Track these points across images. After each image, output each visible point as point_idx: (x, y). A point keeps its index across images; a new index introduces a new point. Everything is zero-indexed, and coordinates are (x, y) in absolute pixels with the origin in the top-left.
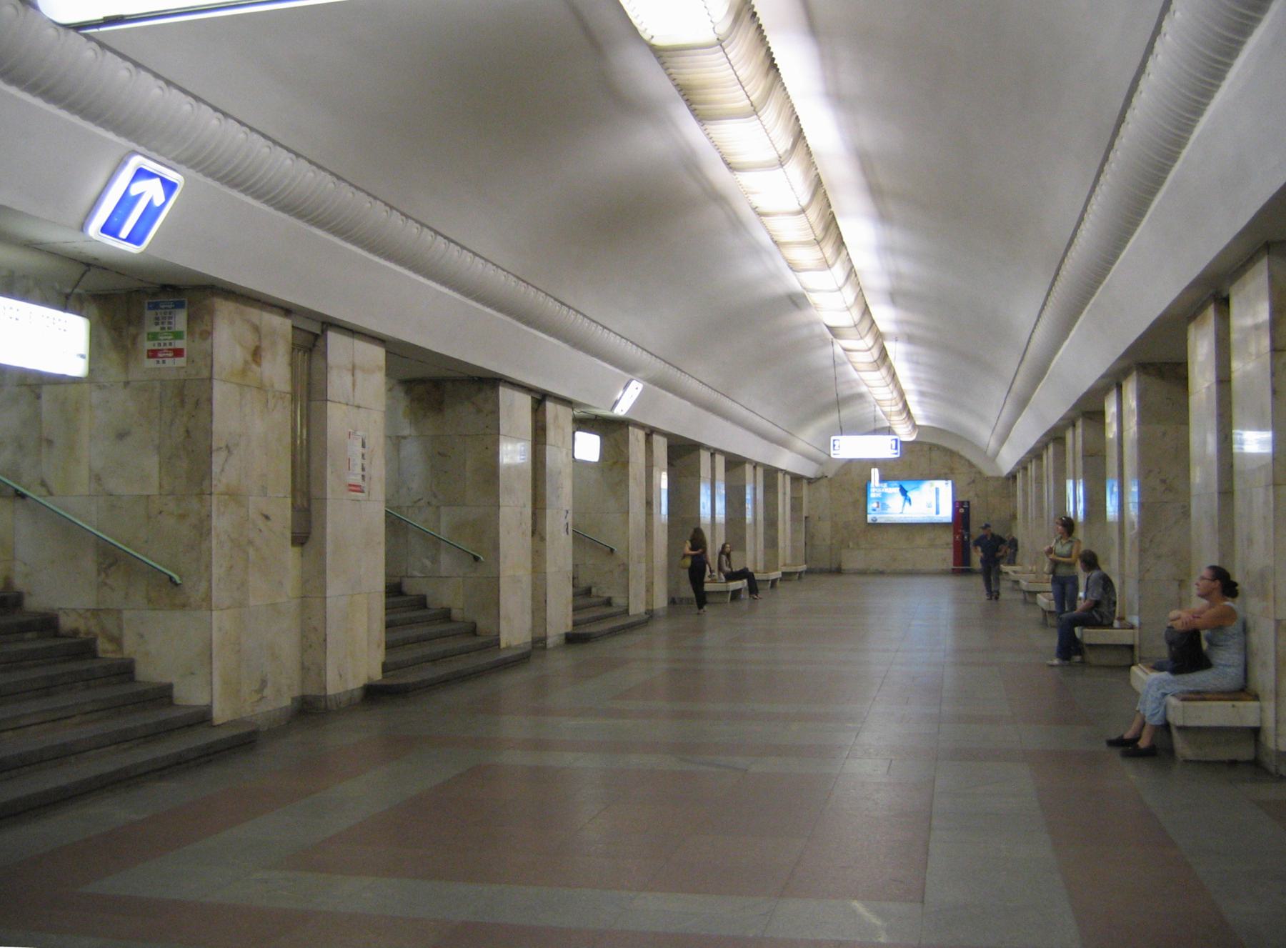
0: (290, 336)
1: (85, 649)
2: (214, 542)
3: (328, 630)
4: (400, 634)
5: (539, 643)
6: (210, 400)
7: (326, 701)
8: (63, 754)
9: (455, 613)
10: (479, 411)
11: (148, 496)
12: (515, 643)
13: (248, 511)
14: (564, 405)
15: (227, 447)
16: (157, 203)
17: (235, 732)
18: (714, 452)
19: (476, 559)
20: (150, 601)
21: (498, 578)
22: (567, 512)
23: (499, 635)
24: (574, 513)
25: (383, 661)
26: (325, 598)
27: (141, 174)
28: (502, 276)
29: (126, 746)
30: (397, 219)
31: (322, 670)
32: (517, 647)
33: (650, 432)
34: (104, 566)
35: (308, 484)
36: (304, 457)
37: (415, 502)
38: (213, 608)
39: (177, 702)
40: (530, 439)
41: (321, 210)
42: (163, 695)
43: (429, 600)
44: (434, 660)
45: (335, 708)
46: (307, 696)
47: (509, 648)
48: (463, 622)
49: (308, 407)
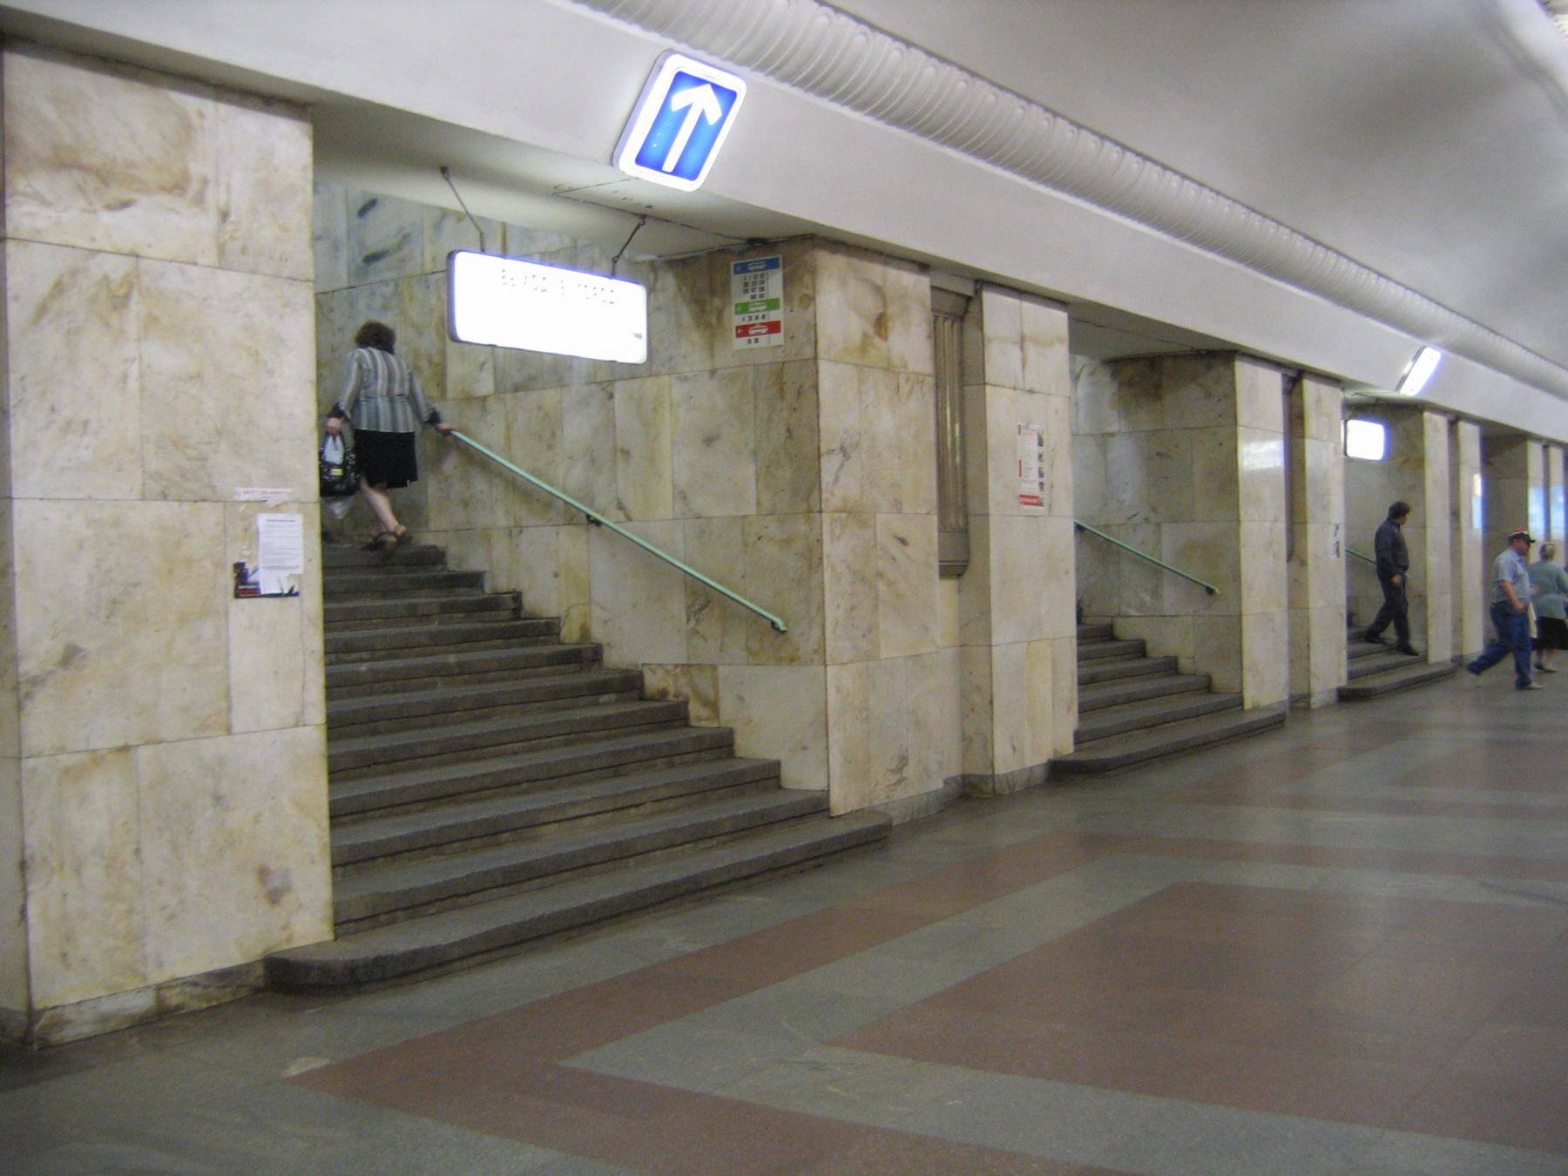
0: (928, 303)
1: (676, 715)
2: (827, 575)
3: (995, 689)
4: (1099, 693)
5: (1300, 704)
6: (816, 387)
7: (994, 784)
8: (619, 855)
9: (1184, 663)
10: (1209, 395)
11: (744, 517)
12: (1266, 701)
13: (875, 533)
14: (1328, 384)
15: (842, 448)
16: (713, 116)
17: (856, 826)
18: (1547, 444)
19: (1210, 591)
20: (751, 652)
21: (1240, 616)
22: (1337, 527)
23: (1241, 692)
24: (1347, 527)
25: (1076, 728)
26: (990, 646)
27: (681, 78)
28: (1225, 206)
29: (708, 844)
30: (1064, 131)
31: (988, 743)
32: (1268, 708)
33: (1455, 420)
34: (694, 609)
35: (965, 495)
36: (958, 459)
37: (1129, 519)
38: (828, 663)
39: (787, 784)
40: (1282, 430)
41: (860, 67)
42: (769, 776)
43: (1149, 646)
44: (1150, 726)
45: (1007, 792)
46: (970, 775)
47: (1256, 708)
48: (1194, 674)
49: (962, 397)
